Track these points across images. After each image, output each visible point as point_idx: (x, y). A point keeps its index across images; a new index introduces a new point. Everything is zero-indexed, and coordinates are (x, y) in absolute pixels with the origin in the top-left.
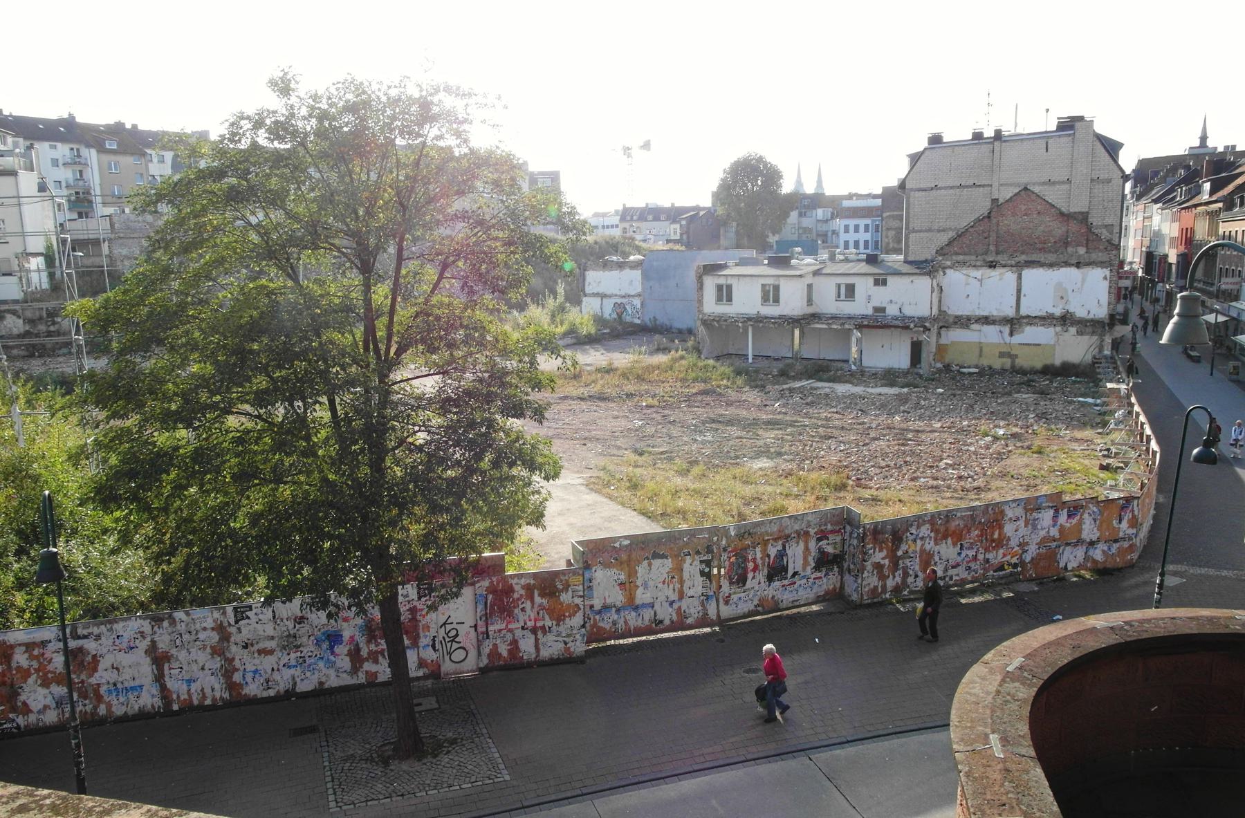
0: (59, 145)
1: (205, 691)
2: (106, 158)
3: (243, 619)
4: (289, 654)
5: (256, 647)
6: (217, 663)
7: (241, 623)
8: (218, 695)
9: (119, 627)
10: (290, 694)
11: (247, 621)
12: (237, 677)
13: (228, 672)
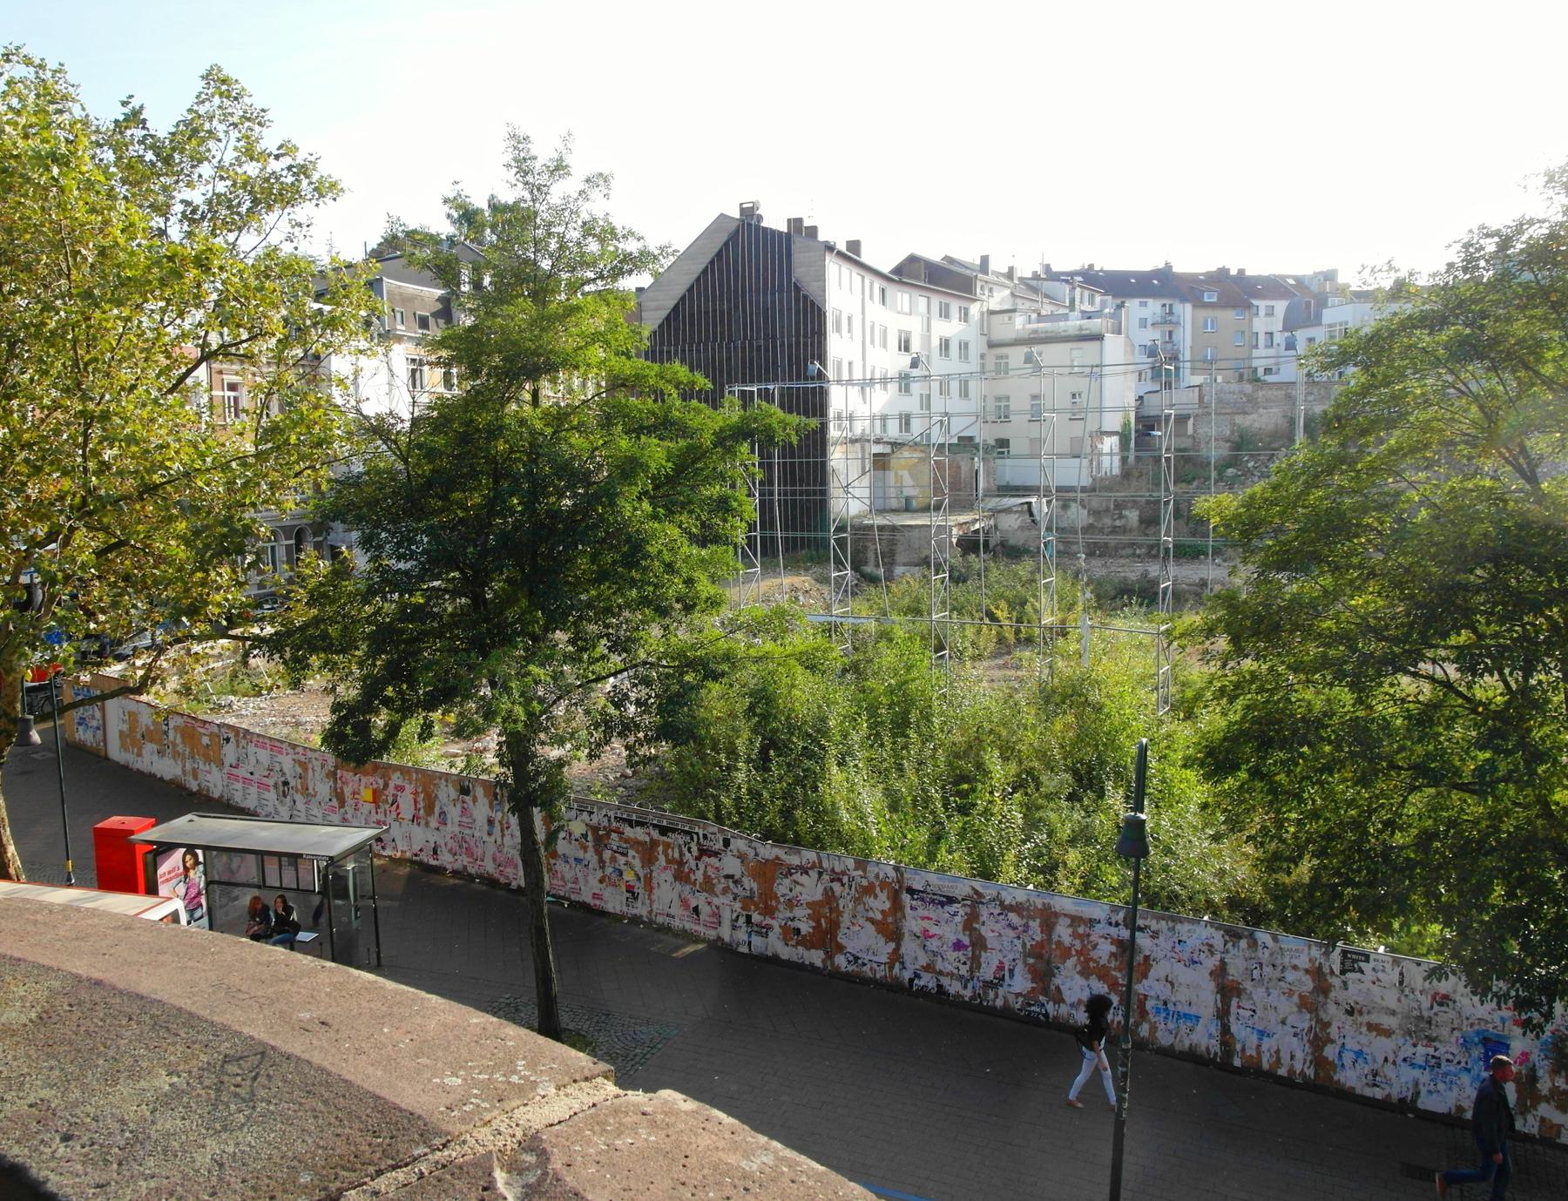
0: (1150, 301)
1: (1282, 1054)
2: (1203, 314)
3: (1353, 970)
4: (1415, 1045)
5: (1366, 1018)
6: (1304, 1022)
7: (1349, 975)
8: (1298, 1067)
9: (1183, 929)
10: (1404, 1106)
11: (1358, 975)
12: (1330, 1052)
13: (1318, 1041)
